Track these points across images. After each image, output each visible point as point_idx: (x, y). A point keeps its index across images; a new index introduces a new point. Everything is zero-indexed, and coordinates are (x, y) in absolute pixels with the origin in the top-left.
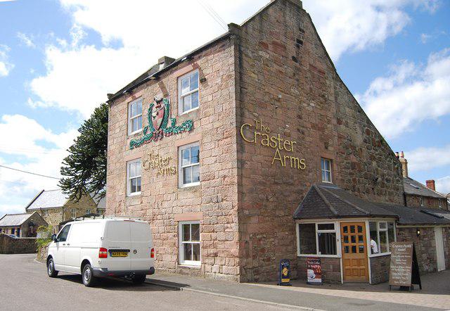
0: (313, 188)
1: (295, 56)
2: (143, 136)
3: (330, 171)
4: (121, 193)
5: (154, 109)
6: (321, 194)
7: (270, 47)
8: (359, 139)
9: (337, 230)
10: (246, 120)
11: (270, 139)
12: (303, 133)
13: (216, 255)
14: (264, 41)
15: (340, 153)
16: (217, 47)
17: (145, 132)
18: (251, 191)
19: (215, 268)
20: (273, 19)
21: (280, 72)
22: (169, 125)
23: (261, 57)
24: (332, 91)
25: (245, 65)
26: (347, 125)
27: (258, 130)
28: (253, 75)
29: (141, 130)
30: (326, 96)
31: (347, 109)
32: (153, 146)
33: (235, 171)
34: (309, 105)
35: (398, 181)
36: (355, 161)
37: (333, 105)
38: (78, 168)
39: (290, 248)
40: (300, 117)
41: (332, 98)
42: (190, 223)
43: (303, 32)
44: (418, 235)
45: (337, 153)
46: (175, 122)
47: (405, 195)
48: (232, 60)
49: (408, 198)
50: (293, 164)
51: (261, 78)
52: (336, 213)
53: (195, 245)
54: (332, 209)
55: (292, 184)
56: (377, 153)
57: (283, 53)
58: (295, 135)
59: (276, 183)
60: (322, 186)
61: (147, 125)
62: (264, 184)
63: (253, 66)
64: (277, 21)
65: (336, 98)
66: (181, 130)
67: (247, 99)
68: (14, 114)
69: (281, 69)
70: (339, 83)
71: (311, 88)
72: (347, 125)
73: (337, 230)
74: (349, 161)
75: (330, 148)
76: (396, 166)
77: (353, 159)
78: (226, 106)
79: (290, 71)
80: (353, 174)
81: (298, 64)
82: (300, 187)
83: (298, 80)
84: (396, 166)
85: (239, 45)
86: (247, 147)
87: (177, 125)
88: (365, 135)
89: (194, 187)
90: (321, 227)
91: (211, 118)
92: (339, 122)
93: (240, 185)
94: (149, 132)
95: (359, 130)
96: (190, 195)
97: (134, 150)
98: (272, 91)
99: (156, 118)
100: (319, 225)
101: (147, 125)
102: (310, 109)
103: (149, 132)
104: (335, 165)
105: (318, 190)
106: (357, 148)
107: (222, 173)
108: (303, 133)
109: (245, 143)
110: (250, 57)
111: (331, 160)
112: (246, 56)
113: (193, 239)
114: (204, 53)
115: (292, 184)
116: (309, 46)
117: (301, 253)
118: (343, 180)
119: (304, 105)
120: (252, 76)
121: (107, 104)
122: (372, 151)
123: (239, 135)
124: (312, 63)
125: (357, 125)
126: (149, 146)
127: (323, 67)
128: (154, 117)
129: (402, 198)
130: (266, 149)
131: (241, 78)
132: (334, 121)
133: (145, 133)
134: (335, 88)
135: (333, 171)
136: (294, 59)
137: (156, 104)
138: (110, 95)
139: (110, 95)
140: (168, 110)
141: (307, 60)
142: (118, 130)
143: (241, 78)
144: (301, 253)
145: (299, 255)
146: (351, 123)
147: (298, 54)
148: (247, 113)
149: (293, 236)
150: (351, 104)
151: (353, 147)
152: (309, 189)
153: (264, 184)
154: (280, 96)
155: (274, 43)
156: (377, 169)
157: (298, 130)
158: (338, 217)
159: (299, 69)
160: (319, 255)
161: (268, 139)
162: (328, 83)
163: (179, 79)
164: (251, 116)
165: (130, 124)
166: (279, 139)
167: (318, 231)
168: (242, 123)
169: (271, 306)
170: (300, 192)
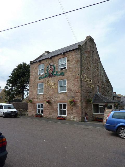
0: (96, 94)
4: (35, 93)
5: (49, 68)
8: (104, 81)
10: (82, 74)
13: (72, 113)
15: (101, 84)
16: (74, 51)
19: (72, 117)
22: (55, 73)
25: (82, 57)
33: (80, 89)
37: (100, 70)
38: (11, 83)
39: (91, 111)
42: (63, 103)
44: (122, 108)
47: (113, 96)
48: (79, 56)
54: (104, 100)
55: (91, 93)
57: (90, 55)
58: (92, 78)
59: (88, 92)
61: (46, 72)
66: (59, 75)
77: (103, 86)
78: (76, 69)
79: (91, 60)
82: (93, 94)
85: (81, 51)
86: (82, 82)
87: (58, 73)
89: (64, 93)
90: (100, 105)
91: (71, 72)
93: (81, 93)
94: (47, 75)
96: (63, 95)
97: (41, 80)
98: (88, 66)
99: (50, 71)
101: (46, 72)
103: (47, 75)
111: (99, 86)
113: (40, 109)
114: (69, 52)
115: (91, 93)
116: (95, 53)
120: (83, 61)
121: (30, 64)
123: (81, 78)
126: (47, 79)
129: (113, 97)
131: (81, 61)
132: (100, 75)
137: (50, 66)
138: (31, 62)
139: (31, 62)
141: (95, 57)
143: (81, 61)
145: (93, 113)
146: (103, 75)
154: (89, 67)
155: (88, 51)
160: (100, 113)
163: (59, 60)
164: (83, 73)
165: (39, 72)
168: (81, 75)
169: (103, 129)
170: (93, 95)
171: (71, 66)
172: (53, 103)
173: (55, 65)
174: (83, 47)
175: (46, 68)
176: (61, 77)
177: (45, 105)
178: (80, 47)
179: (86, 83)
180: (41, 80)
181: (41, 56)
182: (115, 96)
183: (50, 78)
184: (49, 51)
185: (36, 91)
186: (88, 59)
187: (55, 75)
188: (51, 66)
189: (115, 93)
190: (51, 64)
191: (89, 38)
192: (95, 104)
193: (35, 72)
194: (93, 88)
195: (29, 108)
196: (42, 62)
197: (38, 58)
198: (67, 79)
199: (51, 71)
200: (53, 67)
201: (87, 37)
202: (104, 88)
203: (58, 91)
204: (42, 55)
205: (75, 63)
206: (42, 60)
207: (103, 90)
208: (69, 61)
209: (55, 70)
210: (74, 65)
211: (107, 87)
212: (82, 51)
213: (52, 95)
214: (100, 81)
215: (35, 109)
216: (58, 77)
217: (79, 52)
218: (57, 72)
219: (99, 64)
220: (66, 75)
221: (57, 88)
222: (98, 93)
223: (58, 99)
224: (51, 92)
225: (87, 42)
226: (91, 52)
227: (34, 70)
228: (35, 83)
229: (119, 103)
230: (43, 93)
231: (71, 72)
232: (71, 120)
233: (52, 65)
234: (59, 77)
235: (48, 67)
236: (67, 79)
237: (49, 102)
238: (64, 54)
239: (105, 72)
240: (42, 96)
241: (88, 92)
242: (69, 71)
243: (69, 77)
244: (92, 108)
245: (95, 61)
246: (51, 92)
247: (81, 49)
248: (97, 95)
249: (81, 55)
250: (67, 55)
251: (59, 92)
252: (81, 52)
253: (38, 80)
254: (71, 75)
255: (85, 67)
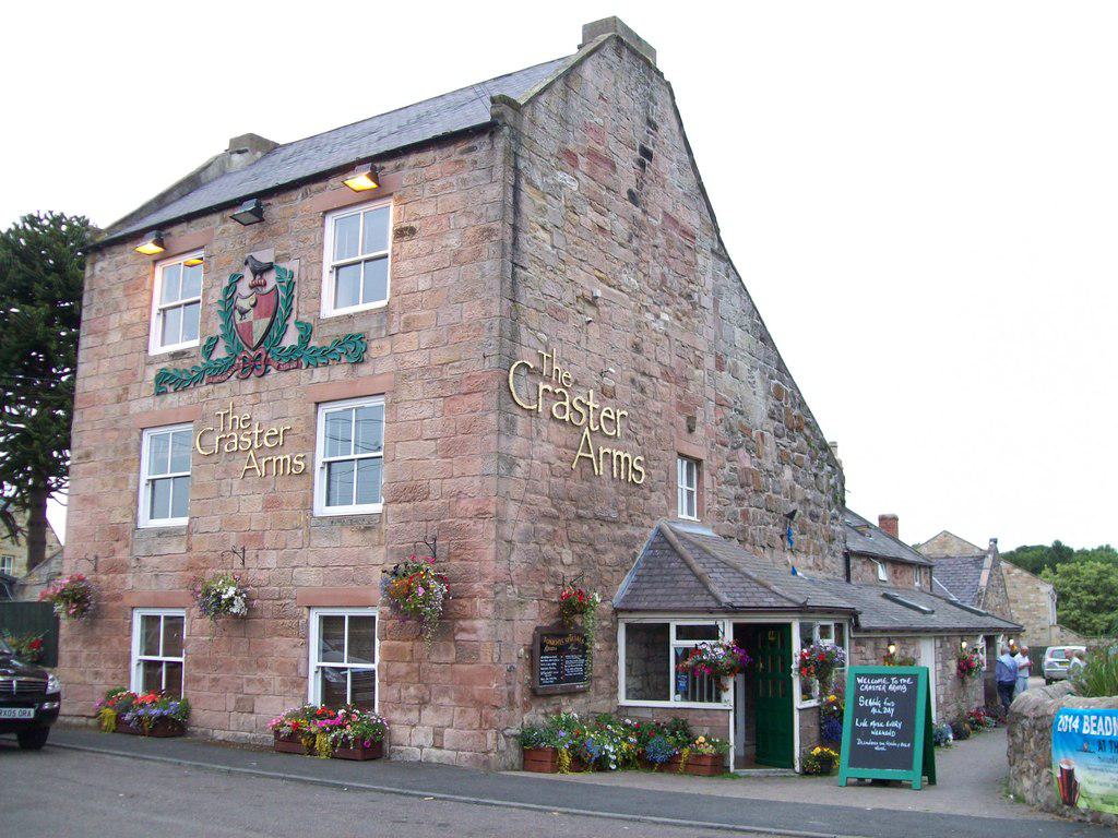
0: (660, 533)
1: (635, 190)
2: (201, 361)
3: (694, 489)
5: (243, 288)
6: (682, 548)
7: (582, 160)
9: (14, 683)
11: (571, 404)
12: (642, 390)
14: (571, 147)
16: (454, 152)
17: (209, 349)
18: (528, 537)
20: (592, 93)
21: (601, 229)
22: (291, 339)
23: (561, 186)
24: (709, 282)
25: (526, 207)
26: (734, 374)
27: (548, 380)
28: (542, 234)
29: (196, 343)
30: (696, 296)
31: (738, 331)
32: (234, 395)
34: (658, 317)
35: (835, 517)
36: (747, 464)
40: (637, 348)
41: (707, 301)
43: (655, 128)
45: (713, 445)
46: (306, 332)
48: (494, 192)
49: (852, 561)
50: (619, 468)
51: (559, 242)
52: (725, 599)
53: (356, 675)
56: (795, 445)
57: (609, 181)
58: (626, 393)
60: (680, 528)
61: (219, 332)
62: (553, 518)
63: (542, 210)
64: (601, 97)
65: (716, 302)
66: (325, 357)
67: (527, 296)
68: (1068, 548)
69: (600, 220)
70: (723, 265)
71: (663, 275)
72: (734, 374)
73: (14, 683)
74: (736, 465)
75: (699, 431)
76: (832, 481)
77: (746, 461)
79: (622, 228)
80: (743, 499)
81: (638, 211)
82: (629, 530)
83: (637, 253)
84: (832, 481)
88: (772, 400)
90: (683, 633)
92: (720, 365)
94: (221, 353)
95: (760, 388)
96: (350, 537)
98: (582, 278)
99: (250, 316)
100: (679, 628)
101: (219, 332)
102: (658, 326)
103: (221, 353)
104: (706, 473)
105: (672, 536)
106: (754, 433)
107: (449, 485)
108: (642, 390)
109: (518, 411)
110: (537, 188)
111: (699, 462)
112: (531, 183)
114: (413, 159)
116: (665, 164)
117: (627, 698)
118: (720, 514)
119: (649, 317)
122: (785, 441)
124: (669, 210)
125: (756, 373)
127: (691, 220)
128: (243, 313)
129: (840, 560)
130: (562, 428)
132: (710, 362)
133: (209, 355)
134: (716, 277)
135: (700, 487)
136: (633, 197)
137: (249, 277)
140: (290, 296)
141: (660, 201)
142: (115, 337)
144: (627, 698)
145: (623, 701)
146: (744, 366)
147: (640, 186)
148: (524, 334)
149: (612, 653)
150: (747, 320)
151: (746, 431)
152: (651, 533)
153: (553, 518)
154: (598, 293)
156: (792, 488)
157: (633, 381)
158: (731, 610)
159: (640, 225)
160: (675, 702)
161: (567, 404)
162: (701, 262)
164: (533, 342)
166: (591, 404)
167: (675, 643)
171: (424, 283)
172: (268, 615)
173: (292, 266)
174: (542, 118)
175: (217, 294)
176: (340, 372)
177: (196, 628)
178: (510, 117)
179: (558, 434)
180: (174, 400)
181: (192, 183)
182: (861, 555)
183: (249, 386)
184: (265, 136)
185: (126, 498)
186: (590, 217)
187: (295, 359)
188: (261, 270)
189: (889, 524)
190: (265, 257)
191: (602, 37)
192: (635, 619)
193: (126, 328)
194: (632, 476)
195: (64, 651)
196: (183, 235)
197: (162, 201)
198: (391, 393)
199: (260, 316)
200: (271, 279)
201: (591, 30)
202: (748, 482)
203: (308, 505)
204: (205, 168)
205: (456, 258)
206: (189, 218)
207: (739, 498)
208: (412, 231)
209: (289, 309)
210: (452, 276)
211: (788, 473)
212: (524, 152)
213: (257, 538)
214: (707, 415)
215: (116, 660)
216: (317, 372)
217: (499, 157)
218: (306, 332)
219: (705, 262)
220: (381, 361)
221: (306, 474)
222: (686, 520)
223: (310, 578)
224: (250, 506)
225: (588, 70)
226: (626, 160)
227: (117, 310)
228: (123, 423)
229: (853, 614)
230: (183, 521)
231: (426, 337)
232: (417, 755)
233: (270, 267)
234: (319, 374)
235: (236, 279)
236: (391, 393)
237: (215, 606)
238: (375, 163)
239: (765, 338)
240: (175, 548)
241: (580, 517)
242: (407, 324)
243: (404, 376)
244: (616, 658)
245: (660, 240)
246: (250, 506)
247: (517, 136)
248: (667, 541)
249: (516, 189)
250: (404, 174)
251: (141, 525)
252: (513, 156)
253: (144, 403)
254: (418, 359)
255: (551, 289)
